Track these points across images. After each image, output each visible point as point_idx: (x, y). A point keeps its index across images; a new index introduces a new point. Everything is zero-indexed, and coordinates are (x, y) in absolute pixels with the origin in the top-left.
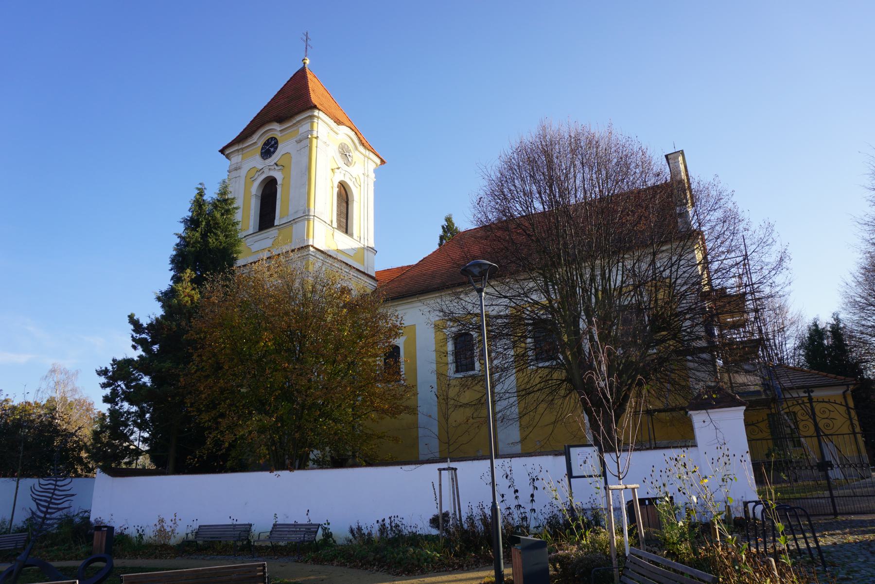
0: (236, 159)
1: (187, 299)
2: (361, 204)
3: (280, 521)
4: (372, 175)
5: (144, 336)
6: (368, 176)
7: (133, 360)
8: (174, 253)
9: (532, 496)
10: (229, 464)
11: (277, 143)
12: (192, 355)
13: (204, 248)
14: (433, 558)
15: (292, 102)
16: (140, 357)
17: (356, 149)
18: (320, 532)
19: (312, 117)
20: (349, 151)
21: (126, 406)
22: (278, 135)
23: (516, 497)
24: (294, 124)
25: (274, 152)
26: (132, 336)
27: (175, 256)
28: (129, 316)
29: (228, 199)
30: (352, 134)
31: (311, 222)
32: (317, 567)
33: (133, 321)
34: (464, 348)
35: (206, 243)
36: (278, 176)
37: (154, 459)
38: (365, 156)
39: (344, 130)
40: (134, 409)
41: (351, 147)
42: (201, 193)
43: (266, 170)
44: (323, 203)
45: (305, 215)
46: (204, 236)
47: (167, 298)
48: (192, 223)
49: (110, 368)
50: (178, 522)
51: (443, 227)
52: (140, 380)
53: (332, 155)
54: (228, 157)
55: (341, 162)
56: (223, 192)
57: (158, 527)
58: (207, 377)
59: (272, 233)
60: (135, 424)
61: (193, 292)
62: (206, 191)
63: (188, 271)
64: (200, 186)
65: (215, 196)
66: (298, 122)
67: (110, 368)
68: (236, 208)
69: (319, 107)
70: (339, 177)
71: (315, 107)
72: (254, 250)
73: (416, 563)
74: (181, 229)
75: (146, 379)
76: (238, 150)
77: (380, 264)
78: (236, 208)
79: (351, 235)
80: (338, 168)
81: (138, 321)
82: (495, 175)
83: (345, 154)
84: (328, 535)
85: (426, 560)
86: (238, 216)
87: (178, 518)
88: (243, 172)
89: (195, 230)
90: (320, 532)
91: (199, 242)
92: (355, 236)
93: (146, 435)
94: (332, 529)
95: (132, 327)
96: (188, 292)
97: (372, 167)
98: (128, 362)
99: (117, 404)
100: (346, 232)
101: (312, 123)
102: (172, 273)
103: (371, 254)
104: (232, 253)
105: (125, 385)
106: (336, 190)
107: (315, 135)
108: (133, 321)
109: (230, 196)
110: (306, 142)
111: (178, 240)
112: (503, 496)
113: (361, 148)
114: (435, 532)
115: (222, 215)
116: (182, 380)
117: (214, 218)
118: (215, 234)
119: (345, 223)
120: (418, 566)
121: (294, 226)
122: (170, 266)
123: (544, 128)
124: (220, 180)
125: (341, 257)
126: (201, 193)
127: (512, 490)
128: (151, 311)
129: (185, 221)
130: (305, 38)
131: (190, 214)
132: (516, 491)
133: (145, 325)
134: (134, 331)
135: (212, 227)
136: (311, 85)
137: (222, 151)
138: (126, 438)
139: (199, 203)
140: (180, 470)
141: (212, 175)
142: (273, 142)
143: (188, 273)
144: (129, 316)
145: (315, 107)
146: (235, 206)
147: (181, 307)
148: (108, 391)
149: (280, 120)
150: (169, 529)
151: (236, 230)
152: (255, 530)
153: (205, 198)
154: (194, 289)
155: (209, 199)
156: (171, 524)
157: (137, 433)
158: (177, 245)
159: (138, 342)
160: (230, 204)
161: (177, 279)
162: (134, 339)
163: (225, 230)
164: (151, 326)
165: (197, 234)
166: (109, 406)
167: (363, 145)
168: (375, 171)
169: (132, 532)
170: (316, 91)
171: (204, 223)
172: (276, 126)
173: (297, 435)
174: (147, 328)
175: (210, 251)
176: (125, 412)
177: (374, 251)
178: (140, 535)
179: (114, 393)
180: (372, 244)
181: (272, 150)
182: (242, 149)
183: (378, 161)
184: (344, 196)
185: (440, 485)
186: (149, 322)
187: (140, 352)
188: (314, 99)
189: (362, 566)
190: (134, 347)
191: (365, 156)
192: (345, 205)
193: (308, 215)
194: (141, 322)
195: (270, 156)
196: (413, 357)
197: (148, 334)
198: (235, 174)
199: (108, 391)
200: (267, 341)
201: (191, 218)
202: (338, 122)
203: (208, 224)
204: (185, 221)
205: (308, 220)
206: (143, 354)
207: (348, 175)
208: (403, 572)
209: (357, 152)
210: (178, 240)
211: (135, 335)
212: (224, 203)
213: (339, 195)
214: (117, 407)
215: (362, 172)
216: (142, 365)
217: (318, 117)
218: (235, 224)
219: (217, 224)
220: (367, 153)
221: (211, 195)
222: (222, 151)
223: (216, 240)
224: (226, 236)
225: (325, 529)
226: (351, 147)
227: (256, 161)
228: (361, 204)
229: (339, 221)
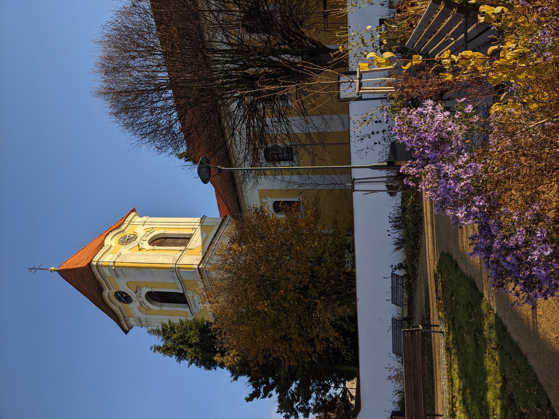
0: (132, 321)
1: (235, 360)
2: (165, 229)
3: (390, 297)
4: (144, 218)
5: (262, 390)
6: (145, 222)
7: (279, 397)
8: (203, 367)
9: (376, 122)
10: (353, 330)
11: (119, 292)
12: (274, 358)
13: (198, 345)
14: (413, 202)
15: (87, 281)
16: (277, 392)
17: (123, 231)
18: (397, 272)
19: (97, 266)
20: (125, 236)
21: (311, 401)
22: (113, 291)
23: (378, 133)
24: (104, 279)
25: (126, 294)
26: (262, 398)
27: (205, 367)
28: (247, 401)
29: (163, 329)
30: (111, 235)
31: (180, 266)
32: (418, 279)
33: (250, 399)
34: (277, 154)
35: (196, 344)
36: (145, 291)
37: (350, 379)
38: (129, 224)
39: (108, 241)
40: (314, 395)
41: (122, 235)
42: (158, 348)
43: (141, 299)
44: (165, 257)
45: (175, 271)
46: (190, 346)
47: (236, 373)
48: (181, 355)
49: (284, 414)
50: (391, 366)
51: (186, 161)
52: (293, 392)
53: (131, 248)
54: (130, 328)
55: (134, 244)
56: (157, 332)
57: (394, 380)
58: (291, 346)
59: (189, 295)
60: (324, 394)
61: (231, 354)
62: (157, 345)
63: (215, 358)
64: (153, 350)
65: (161, 338)
66: (102, 277)
67: (284, 414)
68: (170, 322)
69: (88, 262)
70: (146, 245)
71: (89, 264)
72: (202, 309)
73: (415, 214)
74: (185, 363)
75: (293, 387)
76: (125, 321)
77: (214, 212)
78: (170, 322)
79: (191, 235)
80: (139, 245)
81: (251, 395)
82: (135, 139)
83: (127, 240)
84: (400, 266)
85: (414, 207)
86: (176, 320)
87: (388, 366)
88: (143, 316)
89: (186, 353)
90: (397, 272)
91: (195, 349)
92: (192, 232)
93: (333, 385)
94: (396, 263)
95: (255, 399)
96: (231, 357)
97: (138, 219)
98: (280, 400)
99: (310, 408)
100: (189, 239)
101: (102, 266)
102: (218, 368)
103: (206, 220)
104: (204, 325)
105: (296, 402)
106: (156, 247)
107: (112, 264)
108: (250, 399)
109: (160, 328)
110: (118, 270)
111: (194, 365)
112: (376, 143)
113: (123, 227)
114: (399, 194)
115: (174, 332)
116: (292, 364)
117: (177, 339)
118: (189, 338)
119: (181, 240)
120: (417, 213)
121: (183, 279)
122: (213, 370)
123: (99, 93)
124: (148, 335)
125: (207, 244)
126: (158, 348)
127: (372, 135)
128: (244, 385)
129: (179, 360)
130: (34, 270)
131: (174, 356)
132: (373, 133)
133: (254, 389)
134: (258, 398)
135: (184, 340)
136: (72, 267)
137: (126, 332)
138: (335, 400)
139: (166, 350)
140: (356, 362)
141: (144, 339)
142: (119, 295)
143: (217, 358)
144: (247, 401)
145: (89, 264)
146: (168, 324)
147: (241, 364)
148: (300, 415)
149: (101, 290)
150: (396, 373)
151: (186, 322)
152: (396, 316)
153: (162, 346)
154: (229, 354)
155: (163, 342)
156: (392, 371)
157: (332, 391)
158: (197, 365)
159: (266, 394)
160: (167, 327)
161: (222, 365)
162: (264, 397)
163: (186, 331)
164: (254, 385)
165: (189, 351)
166: (311, 414)
167: (119, 226)
168: (141, 216)
169: (397, 398)
170: (76, 261)
171: (181, 346)
172: (106, 293)
173: (333, 282)
174: (256, 388)
175: (201, 341)
176: (316, 401)
177: (203, 218)
178: (399, 393)
179: (301, 410)
180: (197, 220)
181: (124, 295)
182: (124, 317)
183: (133, 214)
184: (160, 241)
185: (364, 191)
186: (251, 386)
187: (273, 392)
188: (83, 264)
189: (418, 249)
190: (270, 396)
191: (129, 224)
192: (167, 240)
193: (175, 268)
194: (251, 392)
195: (130, 297)
196: (281, 192)
197: (261, 387)
198: (144, 322)
199: (300, 415)
200: (264, 306)
201: (177, 355)
202: (102, 245)
203: (182, 343)
204: (179, 360)
205: (179, 268)
206: (275, 390)
207: (144, 238)
208: (421, 224)
209: (126, 231)
210: (194, 365)
211: (261, 396)
212: (166, 332)
213: (160, 245)
214: (312, 408)
215: (141, 226)
216: (283, 391)
217: (98, 261)
218: (182, 323)
219: (181, 337)
220: (127, 222)
221: (159, 341)
222: (126, 332)
223: (193, 337)
224: (191, 329)
225: (395, 269)
226: (122, 235)
227: (134, 308)
228: (165, 229)
229: (180, 245)
